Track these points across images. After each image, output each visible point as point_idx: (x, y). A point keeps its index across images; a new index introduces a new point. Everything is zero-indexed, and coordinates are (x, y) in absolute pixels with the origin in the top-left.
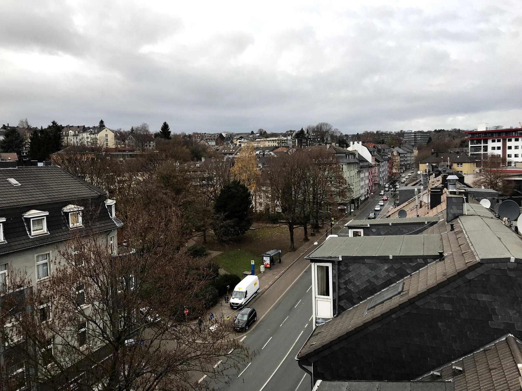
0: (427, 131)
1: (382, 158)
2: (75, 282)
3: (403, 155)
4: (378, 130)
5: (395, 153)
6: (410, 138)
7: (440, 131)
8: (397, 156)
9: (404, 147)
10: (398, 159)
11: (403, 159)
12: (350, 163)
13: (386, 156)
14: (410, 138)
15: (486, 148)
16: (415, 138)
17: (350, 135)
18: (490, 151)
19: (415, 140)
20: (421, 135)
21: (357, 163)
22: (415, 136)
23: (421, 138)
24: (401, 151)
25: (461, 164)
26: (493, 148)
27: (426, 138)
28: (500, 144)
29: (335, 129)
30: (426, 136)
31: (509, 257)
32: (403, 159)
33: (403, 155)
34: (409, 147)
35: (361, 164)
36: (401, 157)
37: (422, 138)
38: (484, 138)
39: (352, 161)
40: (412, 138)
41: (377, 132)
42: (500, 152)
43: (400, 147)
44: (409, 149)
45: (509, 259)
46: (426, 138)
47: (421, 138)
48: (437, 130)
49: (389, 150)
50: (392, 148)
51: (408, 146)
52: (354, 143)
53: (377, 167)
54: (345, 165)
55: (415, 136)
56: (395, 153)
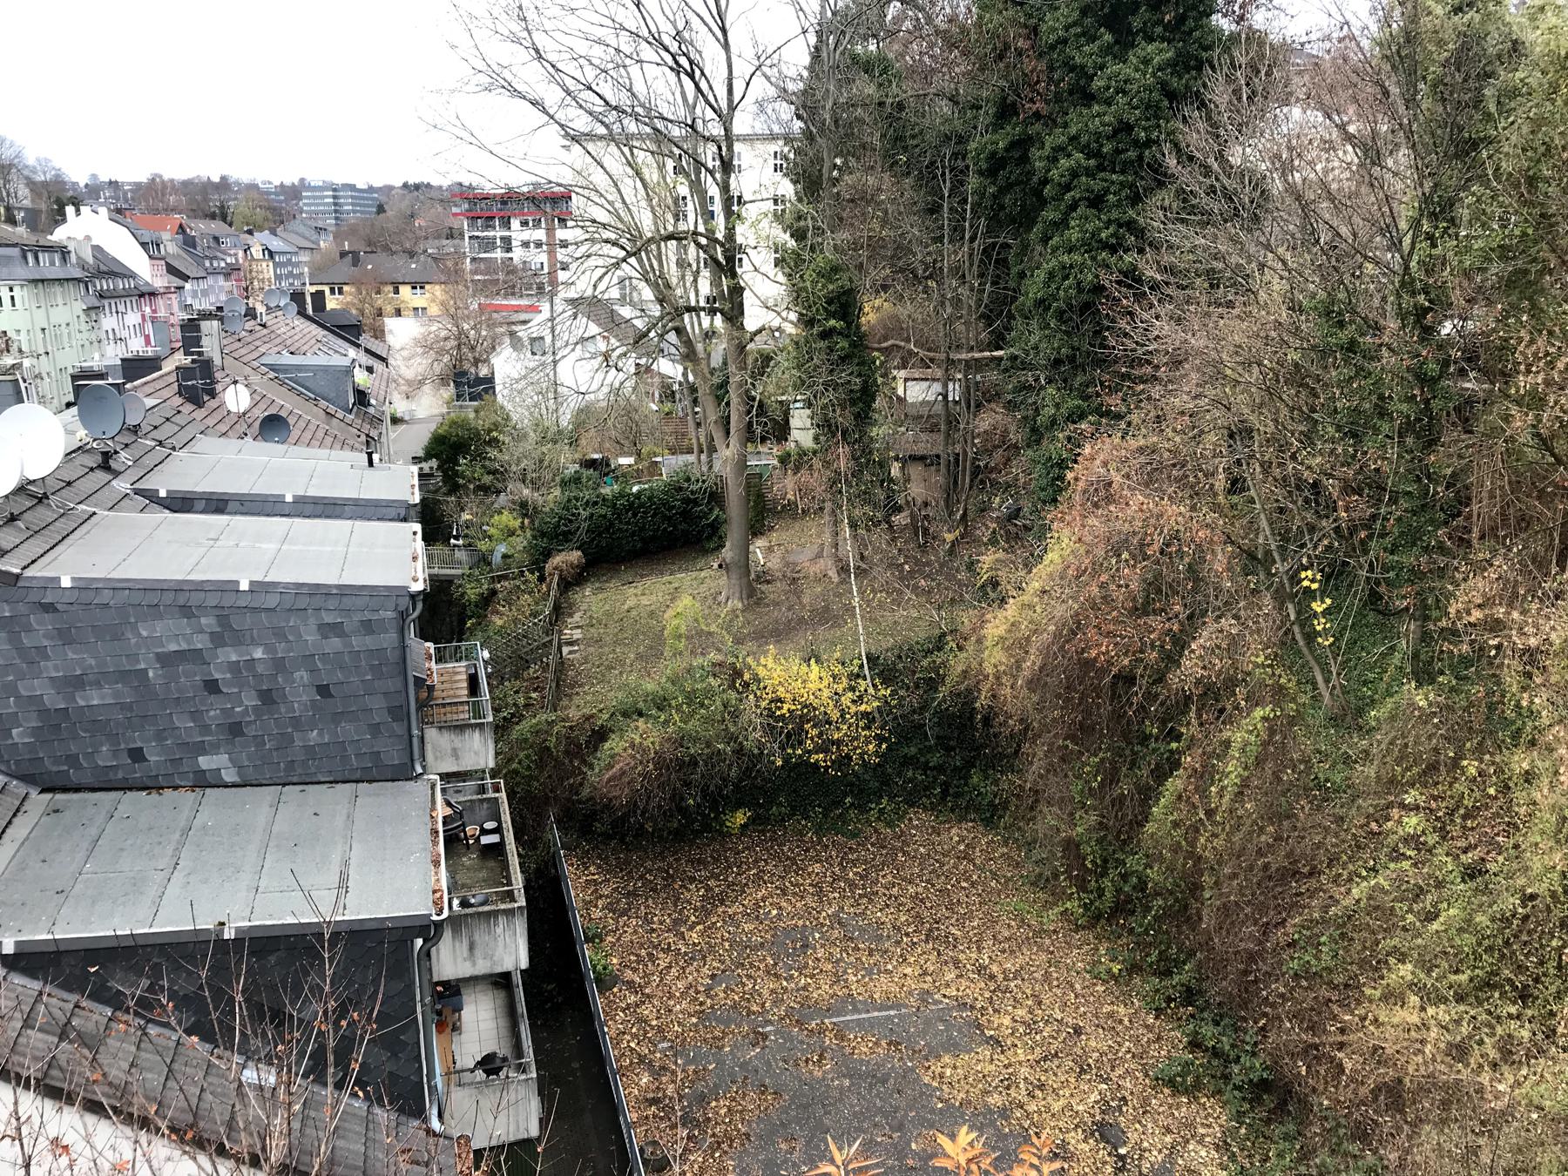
0: (380, 185)
1: (200, 264)
2: (860, 1130)
3: (283, 259)
4: (225, 173)
5: (256, 252)
6: (318, 205)
7: (417, 187)
8: (264, 260)
9: (293, 232)
10: (268, 270)
11: (285, 271)
12: (43, 281)
13: (216, 258)
14: (318, 205)
15: (507, 244)
16: (335, 204)
17: (130, 184)
18: (517, 254)
19: (336, 211)
20: (352, 197)
21: (79, 280)
22: (335, 197)
23: (352, 204)
24: (276, 244)
25: (422, 288)
26: (526, 244)
27: (368, 206)
28: (540, 234)
29: (38, 160)
30: (367, 199)
31: (234, 578)
32: (285, 271)
33: (283, 259)
34: (307, 233)
35: (104, 285)
36: (276, 265)
37: (360, 205)
38: (502, 213)
39: (58, 271)
40: (328, 204)
41: (223, 178)
42: (540, 258)
43: (273, 232)
44: (306, 238)
45: (237, 583)
46: (368, 206)
47: (352, 204)
48: (411, 182)
49: (235, 238)
50: (247, 236)
51: (302, 229)
52: (78, 212)
53: (173, 296)
54: (22, 286)
55: (335, 197)
56: (256, 252)
